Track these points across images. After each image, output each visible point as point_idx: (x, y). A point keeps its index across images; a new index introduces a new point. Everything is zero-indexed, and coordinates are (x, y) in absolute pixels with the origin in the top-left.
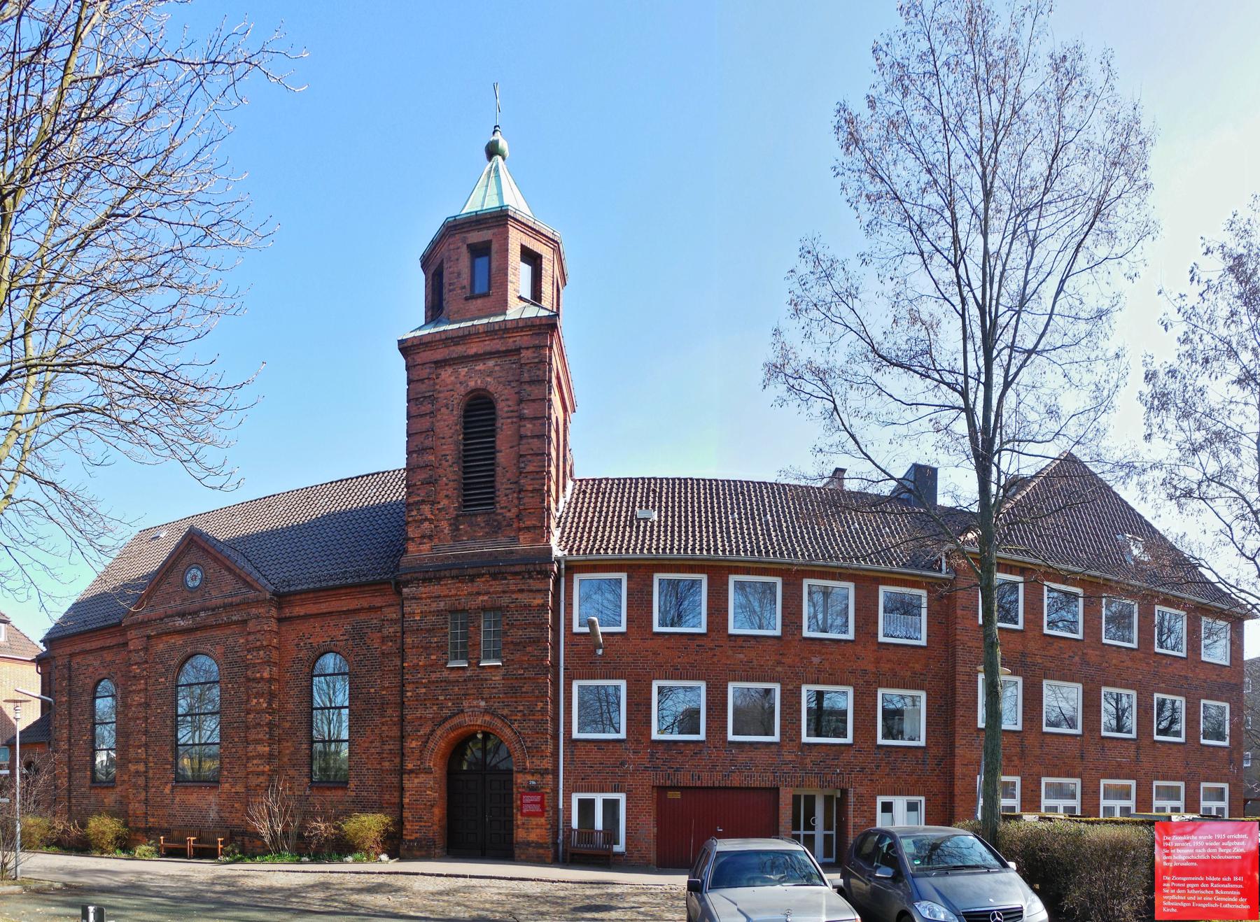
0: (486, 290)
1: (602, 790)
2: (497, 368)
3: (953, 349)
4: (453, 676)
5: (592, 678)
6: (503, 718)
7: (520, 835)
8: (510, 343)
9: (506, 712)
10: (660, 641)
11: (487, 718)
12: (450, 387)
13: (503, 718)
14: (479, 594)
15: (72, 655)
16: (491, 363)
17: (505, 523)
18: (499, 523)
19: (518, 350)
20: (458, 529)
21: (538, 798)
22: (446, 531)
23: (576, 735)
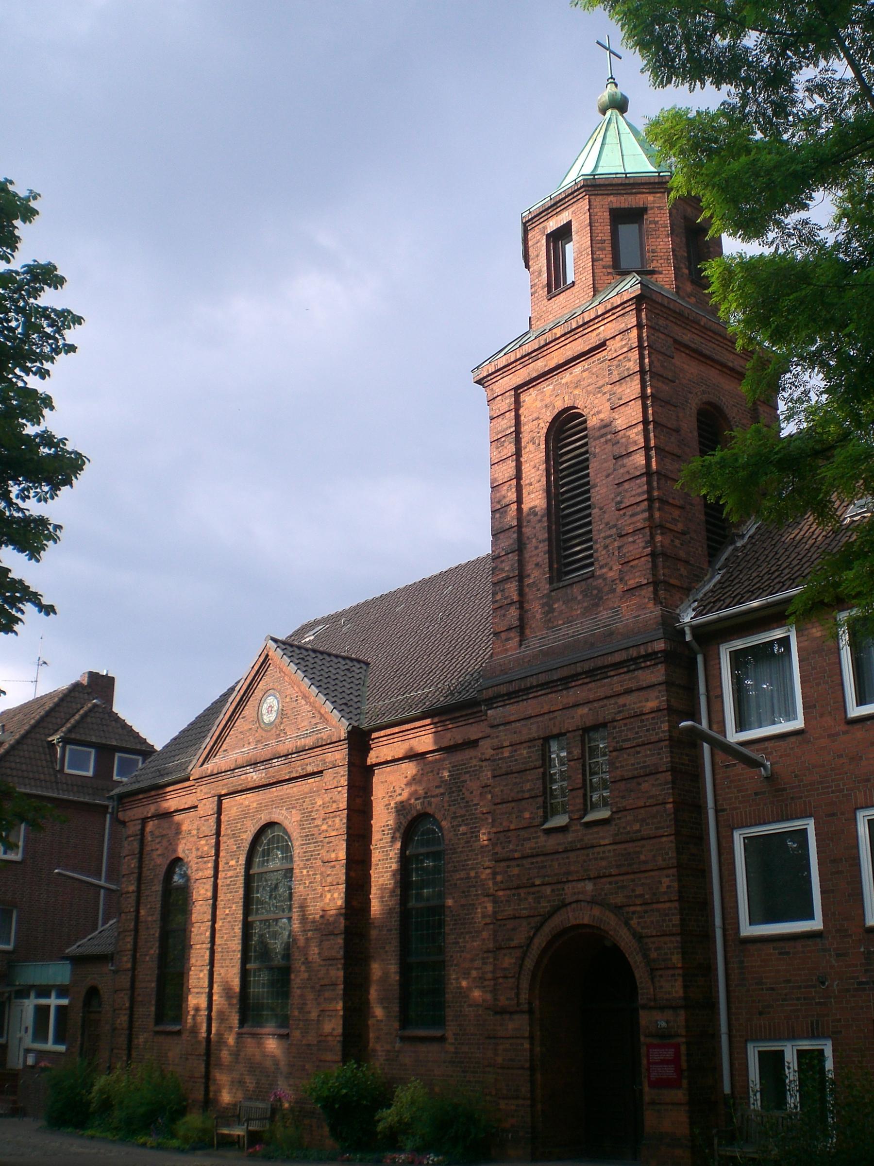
0: (226, 802)
1: (793, 1036)
2: (585, 374)
3: (382, 755)
4: (551, 843)
5: (765, 823)
6: (617, 909)
7: (650, 1119)
8: (593, 340)
9: (619, 900)
10: (859, 733)
11: (596, 911)
12: (535, 415)
13: (617, 909)
14: (576, 705)
15: (518, 390)
16: (577, 370)
17: (606, 589)
18: (600, 591)
19: (602, 345)
20: (552, 610)
21: (670, 1054)
22: (538, 616)
23: (747, 930)
